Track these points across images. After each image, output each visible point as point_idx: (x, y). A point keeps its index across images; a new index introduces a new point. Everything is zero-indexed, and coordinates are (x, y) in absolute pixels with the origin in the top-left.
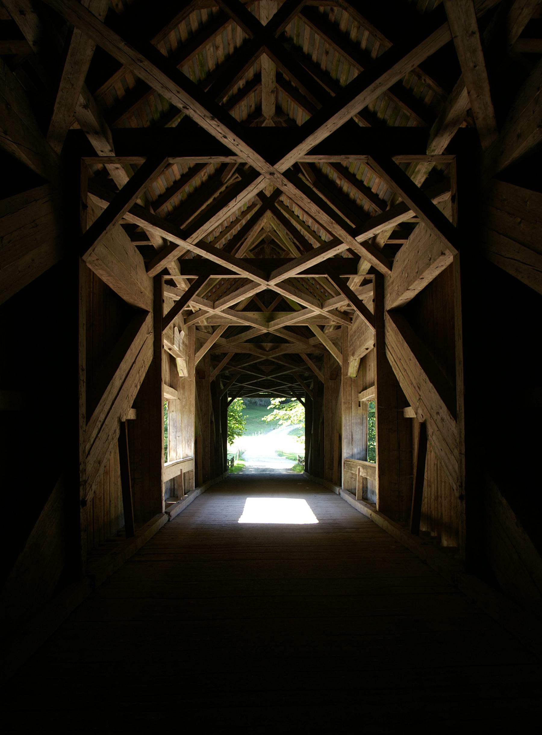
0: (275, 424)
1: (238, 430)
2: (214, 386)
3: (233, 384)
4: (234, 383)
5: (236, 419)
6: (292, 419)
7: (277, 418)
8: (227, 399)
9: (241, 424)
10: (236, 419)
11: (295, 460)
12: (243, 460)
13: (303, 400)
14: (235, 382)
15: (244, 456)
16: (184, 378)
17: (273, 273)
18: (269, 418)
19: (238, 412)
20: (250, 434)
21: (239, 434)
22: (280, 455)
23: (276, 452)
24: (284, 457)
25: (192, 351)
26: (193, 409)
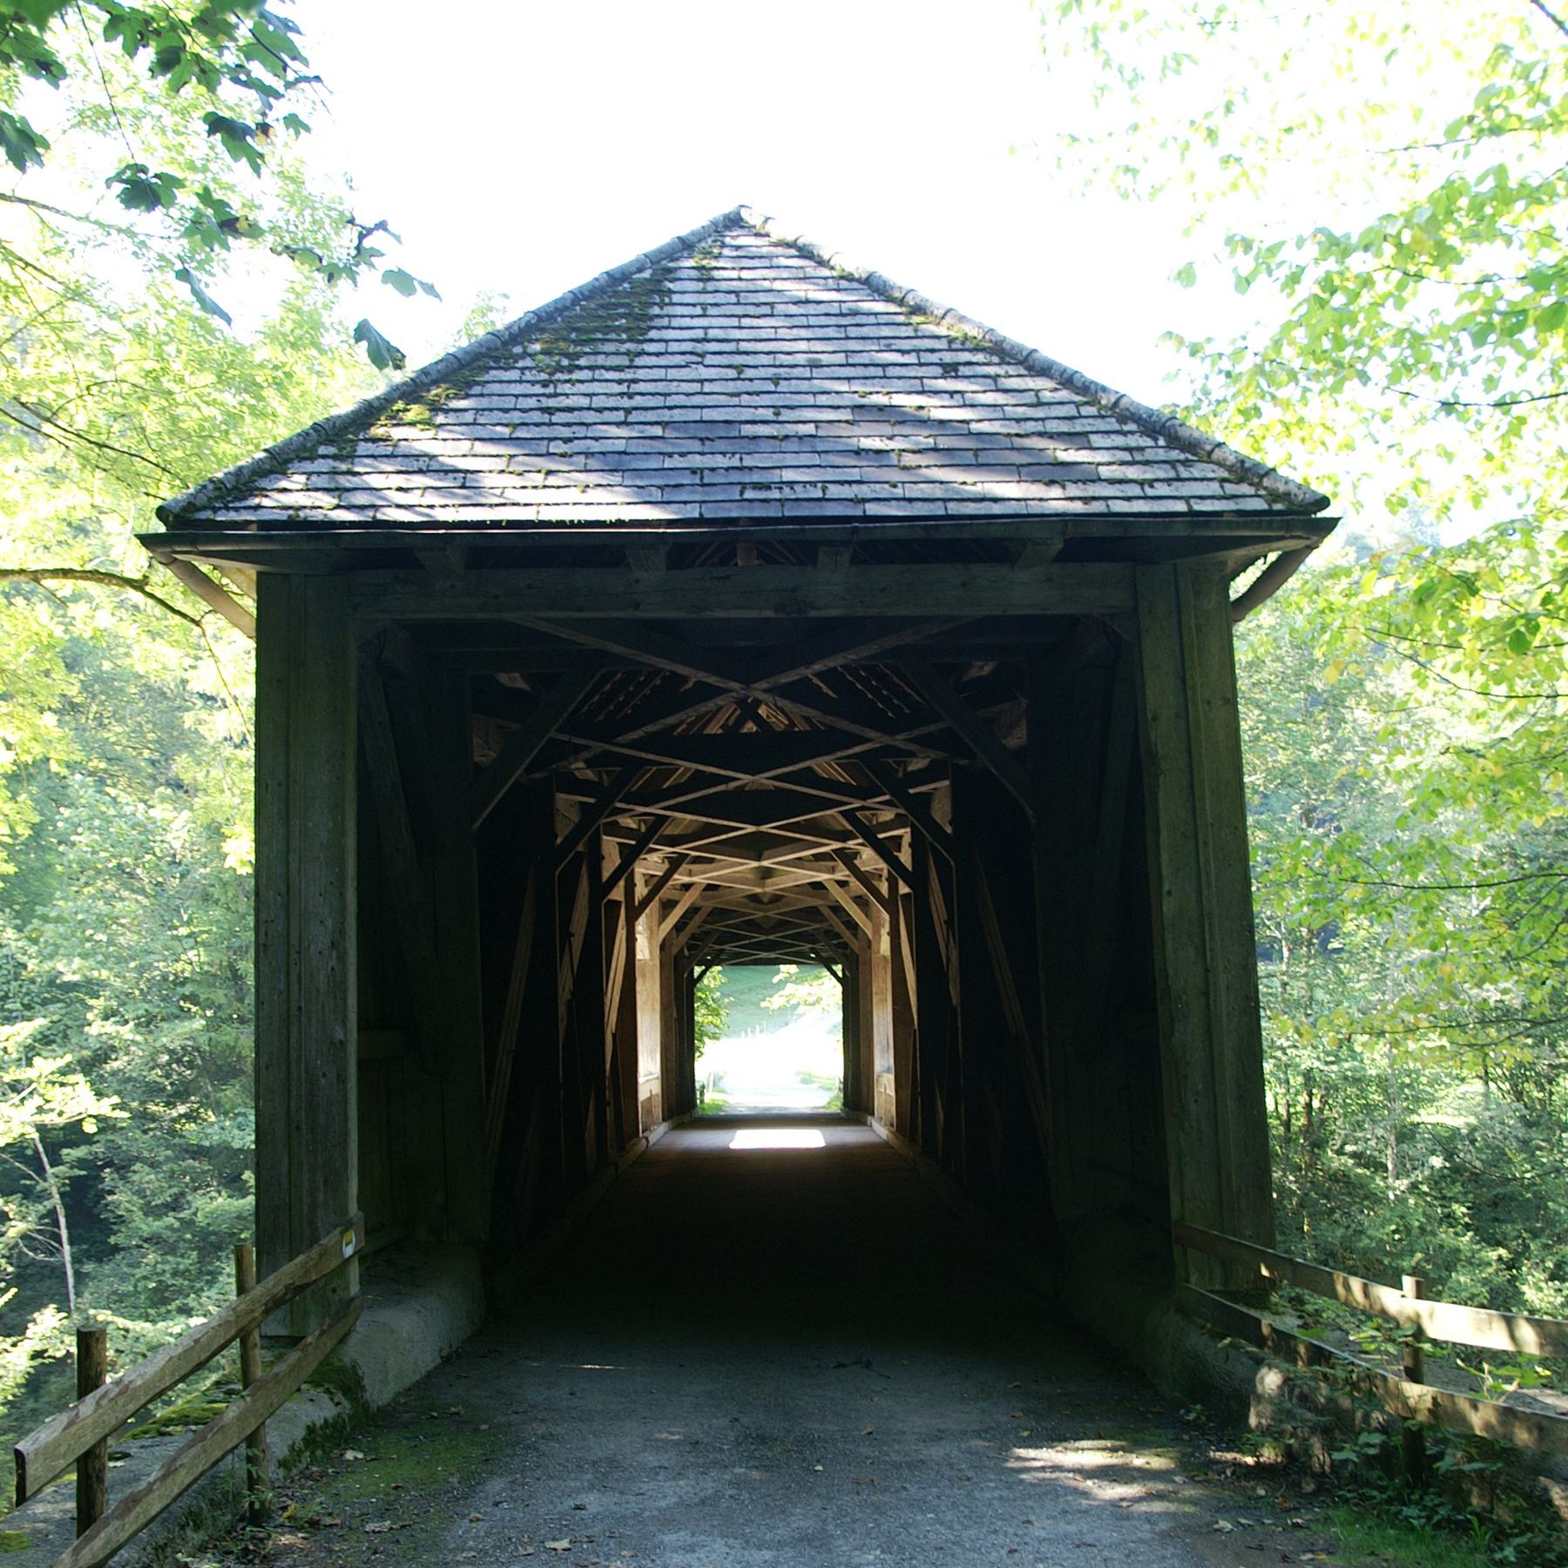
0: (788, 1011)
1: (711, 1029)
2: (678, 957)
3: (551, 739)
4: (552, 734)
5: (708, 1007)
6: (823, 1003)
7: (794, 1001)
8: (692, 971)
9: (718, 1015)
10: (708, 1007)
11: (830, 1089)
12: (722, 1091)
13: (838, 969)
14: (558, 731)
15: (722, 1084)
16: (644, 961)
17: (766, 853)
18: (777, 1001)
19: (711, 991)
20: (736, 1033)
21: (714, 1037)
22: (804, 1081)
23: (57, 87)
24: (815, 1086)
25: (655, 922)
26: (658, 1006)
